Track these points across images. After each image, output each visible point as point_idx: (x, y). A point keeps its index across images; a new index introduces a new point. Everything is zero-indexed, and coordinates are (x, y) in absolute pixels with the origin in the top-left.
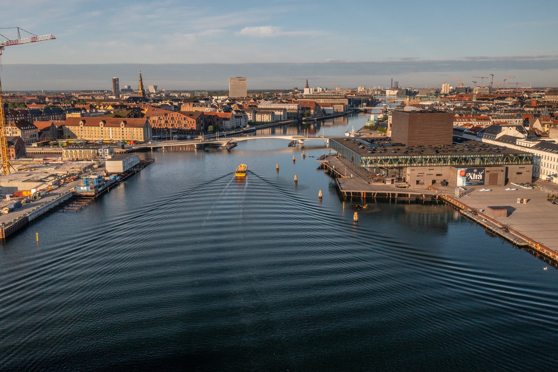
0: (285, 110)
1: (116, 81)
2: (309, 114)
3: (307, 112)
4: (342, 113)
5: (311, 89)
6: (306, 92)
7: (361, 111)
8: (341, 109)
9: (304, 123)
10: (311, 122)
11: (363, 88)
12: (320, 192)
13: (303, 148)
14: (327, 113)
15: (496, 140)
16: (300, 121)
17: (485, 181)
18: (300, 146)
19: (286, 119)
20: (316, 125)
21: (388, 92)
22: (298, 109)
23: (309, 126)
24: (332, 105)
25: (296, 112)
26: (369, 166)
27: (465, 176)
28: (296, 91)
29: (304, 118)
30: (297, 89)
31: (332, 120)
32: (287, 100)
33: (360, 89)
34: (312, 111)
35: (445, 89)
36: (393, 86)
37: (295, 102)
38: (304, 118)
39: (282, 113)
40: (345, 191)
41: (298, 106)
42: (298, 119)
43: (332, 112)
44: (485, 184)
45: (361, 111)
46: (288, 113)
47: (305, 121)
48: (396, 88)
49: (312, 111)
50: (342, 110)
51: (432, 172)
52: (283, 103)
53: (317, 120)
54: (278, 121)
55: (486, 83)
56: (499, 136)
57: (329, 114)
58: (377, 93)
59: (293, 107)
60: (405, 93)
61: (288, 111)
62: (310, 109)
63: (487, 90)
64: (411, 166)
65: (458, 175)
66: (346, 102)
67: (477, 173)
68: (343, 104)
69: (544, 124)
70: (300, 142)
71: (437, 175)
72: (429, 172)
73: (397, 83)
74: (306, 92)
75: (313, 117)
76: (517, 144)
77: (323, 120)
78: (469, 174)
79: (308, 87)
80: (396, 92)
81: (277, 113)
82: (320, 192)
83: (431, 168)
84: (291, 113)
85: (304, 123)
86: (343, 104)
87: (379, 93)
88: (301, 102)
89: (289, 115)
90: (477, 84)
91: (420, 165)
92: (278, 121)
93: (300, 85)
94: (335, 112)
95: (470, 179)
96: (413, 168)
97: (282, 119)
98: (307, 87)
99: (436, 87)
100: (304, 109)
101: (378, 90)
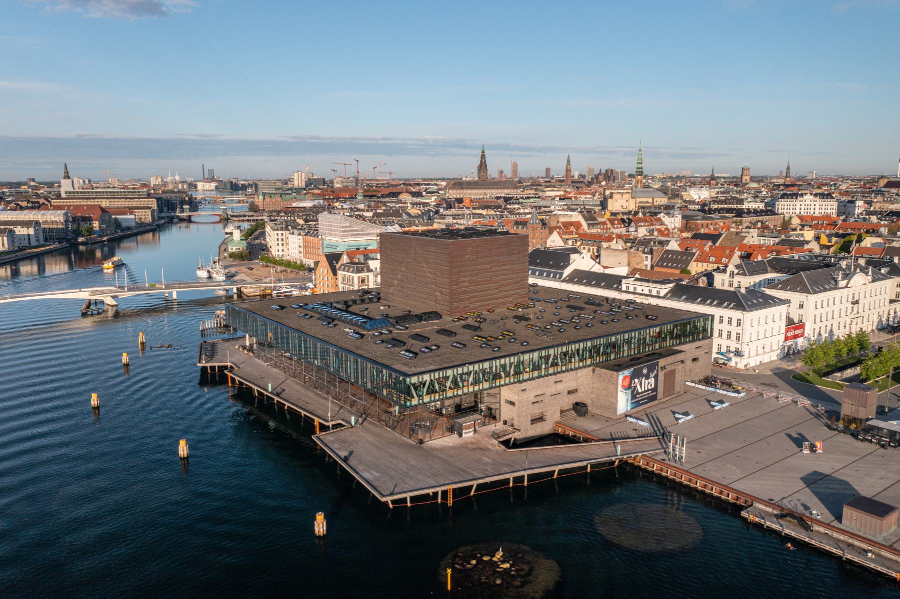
0: (37, 223)
1: (548, 170)
2: (90, 231)
3: (84, 226)
4: (149, 224)
5: (75, 180)
6: (66, 186)
7: (181, 220)
8: (146, 216)
9: (82, 248)
10: (96, 245)
11: (160, 180)
12: (182, 443)
13: (117, 315)
14: (124, 225)
15: (564, 281)
16: (76, 245)
17: (659, 390)
18: (110, 313)
19: (42, 242)
20: (106, 249)
21: (200, 186)
22: (66, 221)
23: (92, 253)
24: (130, 210)
25: (60, 226)
26: (426, 399)
27: (629, 387)
28: (32, 183)
29: (81, 240)
30: (33, 180)
31: (134, 238)
32: (29, 202)
33: (154, 182)
34: (96, 224)
35: (298, 181)
36: (207, 176)
37: (57, 208)
38: (81, 240)
39: (31, 231)
40: (389, 499)
41: (66, 214)
42: (68, 241)
43: (133, 224)
44: (659, 396)
45: (181, 220)
46: (44, 230)
47: (83, 244)
48: (211, 179)
49: (96, 224)
50: (149, 219)
51: (560, 387)
52: (22, 208)
53: (108, 240)
54: (26, 248)
55: (351, 172)
56: (567, 272)
57: (128, 228)
58: (183, 186)
59: (54, 218)
60: (229, 186)
61: (43, 226)
62: (90, 219)
63: (352, 181)
64: (519, 382)
65: (620, 388)
66: (154, 204)
67: (647, 377)
68: (149, 208)
69: (568, 239)
70: (109, 301)
71: (569, 392)
72: (554, 389)
73: (211, 171)
74: (66, 186)
75: (99, 236)
76: (624, 288)
77: (120, 240)
78: (636, 380)
79: (69, 178)
80: (213, 185)
81: (20, 231)
82: (182, 443)
83: (559, 377)
84: (51, 230)
85: (82, 248)
86: (149, 208)
87: (185, 187)
88: (69, 206)
89: (49, 235)
90: (337, 174)
91: (536, 374)
92: (26, 248)
93: (55, 174)
94: (137, 223)
95: (638, 393)
96: (523, 386)
97: (34, 243)
98: (67, 177)
99: (284, 177)
100: (78, 221)
101: (183, 182)
